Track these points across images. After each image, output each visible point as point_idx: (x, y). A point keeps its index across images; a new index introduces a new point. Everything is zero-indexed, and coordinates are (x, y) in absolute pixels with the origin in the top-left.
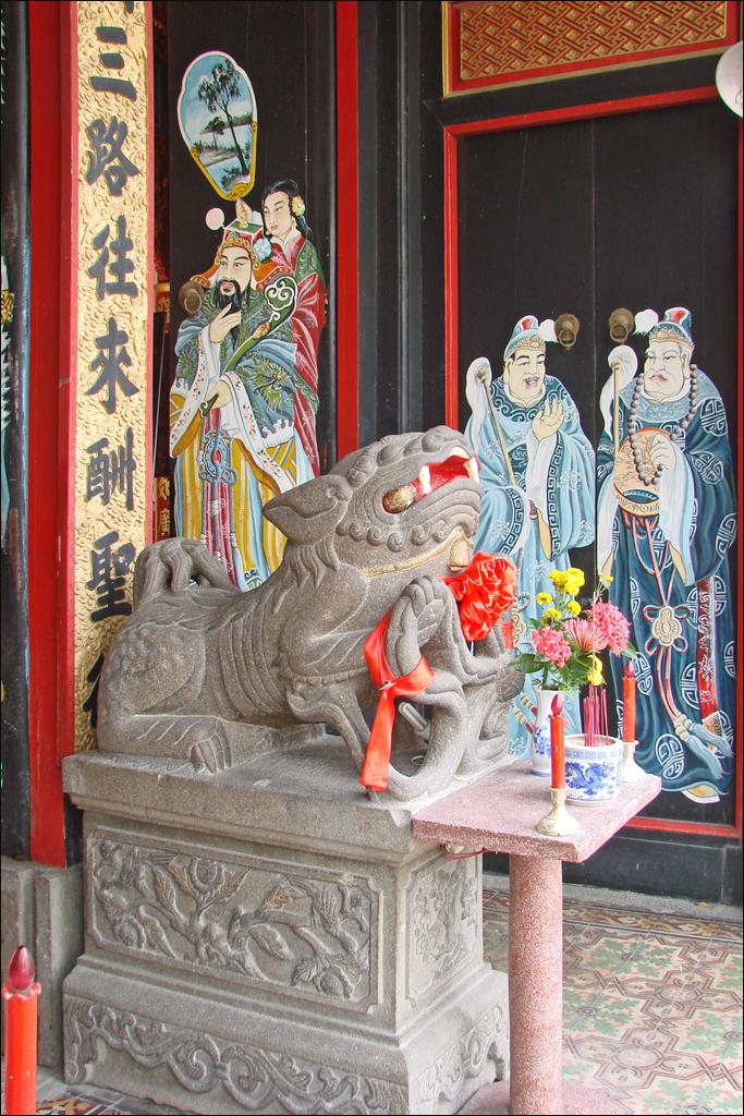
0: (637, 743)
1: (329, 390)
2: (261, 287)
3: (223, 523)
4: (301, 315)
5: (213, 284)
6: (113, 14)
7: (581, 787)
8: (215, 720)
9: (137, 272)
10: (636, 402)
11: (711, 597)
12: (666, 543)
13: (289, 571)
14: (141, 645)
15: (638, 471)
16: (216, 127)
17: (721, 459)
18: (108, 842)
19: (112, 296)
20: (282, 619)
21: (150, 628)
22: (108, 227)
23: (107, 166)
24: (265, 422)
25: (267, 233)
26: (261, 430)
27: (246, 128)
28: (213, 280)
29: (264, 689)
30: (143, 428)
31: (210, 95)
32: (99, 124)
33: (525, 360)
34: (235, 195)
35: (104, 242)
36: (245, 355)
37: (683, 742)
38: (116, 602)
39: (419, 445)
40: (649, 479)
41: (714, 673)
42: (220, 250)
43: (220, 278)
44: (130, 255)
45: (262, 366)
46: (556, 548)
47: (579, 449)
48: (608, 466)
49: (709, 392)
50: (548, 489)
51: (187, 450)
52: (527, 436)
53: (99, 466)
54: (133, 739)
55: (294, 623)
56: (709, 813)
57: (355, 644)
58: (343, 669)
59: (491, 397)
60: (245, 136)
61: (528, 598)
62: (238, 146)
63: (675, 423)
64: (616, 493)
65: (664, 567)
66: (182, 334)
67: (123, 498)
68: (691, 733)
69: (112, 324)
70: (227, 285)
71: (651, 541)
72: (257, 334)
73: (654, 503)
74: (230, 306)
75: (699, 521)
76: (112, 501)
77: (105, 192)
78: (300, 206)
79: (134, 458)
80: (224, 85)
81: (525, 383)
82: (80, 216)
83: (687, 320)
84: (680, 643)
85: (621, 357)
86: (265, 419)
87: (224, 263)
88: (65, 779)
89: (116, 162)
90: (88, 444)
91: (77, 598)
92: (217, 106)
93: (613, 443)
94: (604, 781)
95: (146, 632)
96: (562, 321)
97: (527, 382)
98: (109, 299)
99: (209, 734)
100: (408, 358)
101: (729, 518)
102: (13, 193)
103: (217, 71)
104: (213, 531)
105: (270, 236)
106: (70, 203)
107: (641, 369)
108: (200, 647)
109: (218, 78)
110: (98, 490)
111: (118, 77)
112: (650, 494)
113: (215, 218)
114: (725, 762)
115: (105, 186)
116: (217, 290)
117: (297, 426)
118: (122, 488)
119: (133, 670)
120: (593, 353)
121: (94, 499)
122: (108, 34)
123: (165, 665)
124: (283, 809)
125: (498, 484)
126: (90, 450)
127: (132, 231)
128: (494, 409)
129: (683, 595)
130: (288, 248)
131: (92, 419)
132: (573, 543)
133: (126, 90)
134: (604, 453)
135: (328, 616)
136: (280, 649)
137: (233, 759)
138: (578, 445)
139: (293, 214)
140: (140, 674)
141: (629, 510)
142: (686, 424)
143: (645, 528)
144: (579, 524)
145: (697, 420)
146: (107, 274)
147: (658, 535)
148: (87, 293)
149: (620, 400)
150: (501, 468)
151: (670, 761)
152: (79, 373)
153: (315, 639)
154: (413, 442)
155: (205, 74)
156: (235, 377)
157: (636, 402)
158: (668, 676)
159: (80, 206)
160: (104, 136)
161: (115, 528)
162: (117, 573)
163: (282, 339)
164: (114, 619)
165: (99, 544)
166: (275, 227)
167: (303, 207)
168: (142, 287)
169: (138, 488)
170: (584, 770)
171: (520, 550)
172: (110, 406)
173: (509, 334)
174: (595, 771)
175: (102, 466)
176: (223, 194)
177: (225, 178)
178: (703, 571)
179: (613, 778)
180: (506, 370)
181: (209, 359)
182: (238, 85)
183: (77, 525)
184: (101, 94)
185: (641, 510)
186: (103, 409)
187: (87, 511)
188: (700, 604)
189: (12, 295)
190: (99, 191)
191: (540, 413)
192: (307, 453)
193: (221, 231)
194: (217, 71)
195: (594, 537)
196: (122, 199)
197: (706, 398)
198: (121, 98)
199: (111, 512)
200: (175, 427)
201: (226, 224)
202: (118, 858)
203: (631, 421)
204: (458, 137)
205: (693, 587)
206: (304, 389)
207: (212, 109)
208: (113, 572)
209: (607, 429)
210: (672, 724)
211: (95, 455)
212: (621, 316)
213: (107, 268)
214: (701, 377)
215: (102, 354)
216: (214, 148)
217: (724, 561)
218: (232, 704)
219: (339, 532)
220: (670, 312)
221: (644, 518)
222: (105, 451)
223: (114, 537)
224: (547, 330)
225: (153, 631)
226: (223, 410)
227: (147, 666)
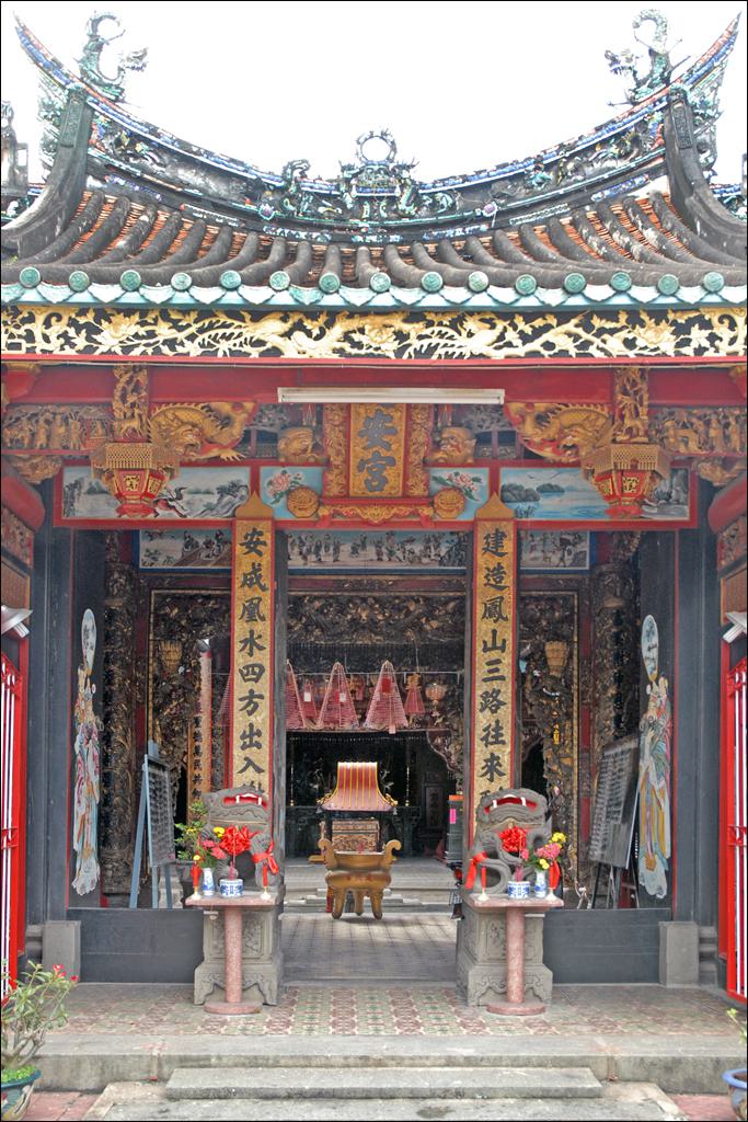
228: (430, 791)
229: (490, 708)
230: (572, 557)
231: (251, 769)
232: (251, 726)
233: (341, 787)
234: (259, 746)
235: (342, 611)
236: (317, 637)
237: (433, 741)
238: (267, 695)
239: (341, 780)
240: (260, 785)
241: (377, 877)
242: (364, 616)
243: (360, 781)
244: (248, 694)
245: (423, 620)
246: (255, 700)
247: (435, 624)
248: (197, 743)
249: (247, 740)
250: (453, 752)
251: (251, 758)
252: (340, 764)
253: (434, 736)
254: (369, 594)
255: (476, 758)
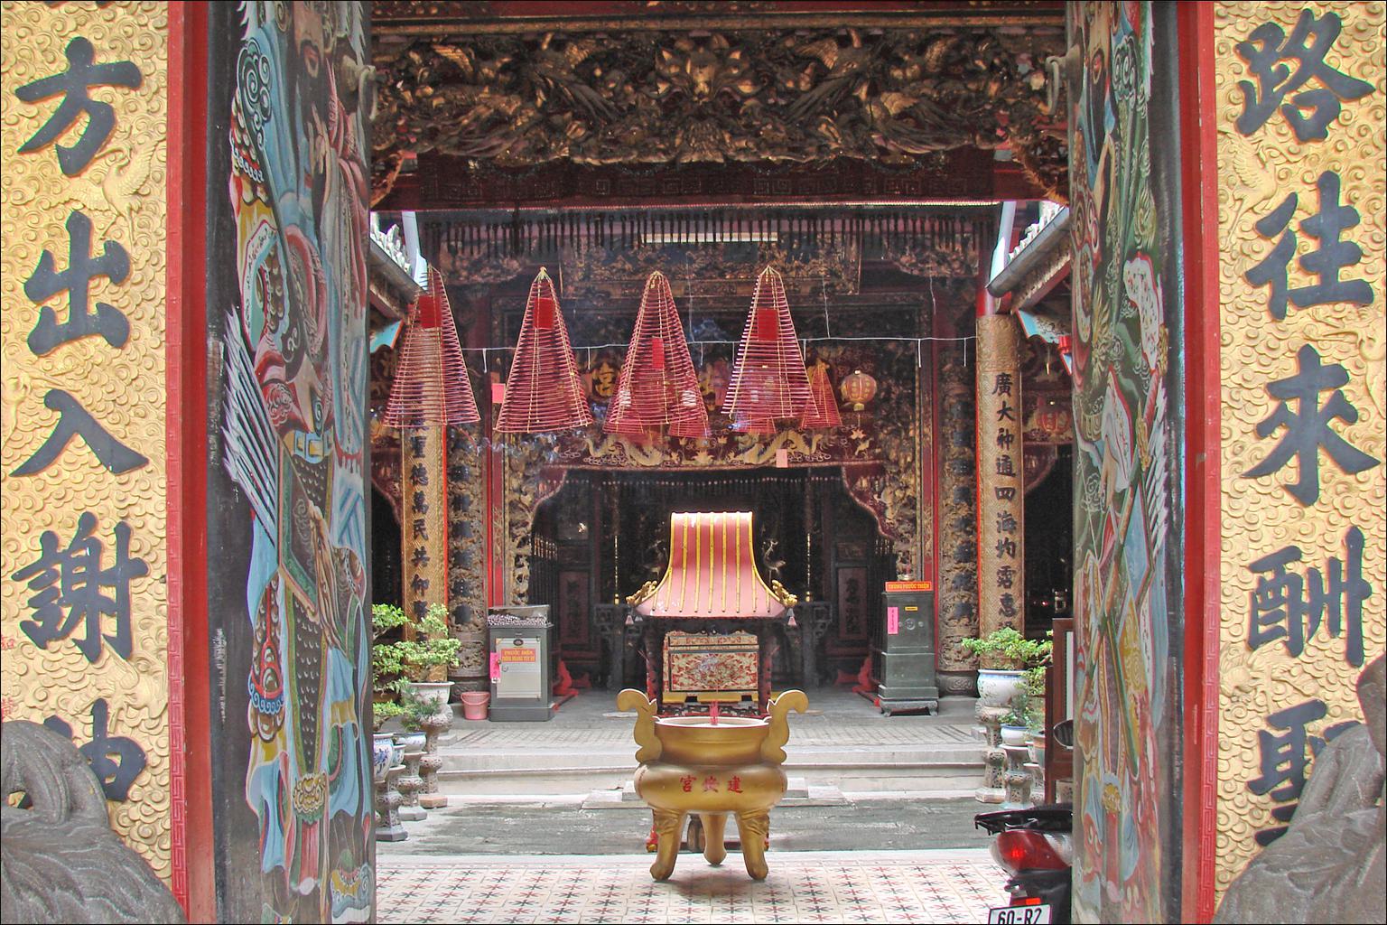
89: (1313, 84)
115: (1285, 129)
118: (1334, 630)
222: (1292, 567)
228: (844, 576)
229: (1291, 116)
231: (79, 450)
232: (79, 226)
233: (678, 565)
234: (116, 329)
235: (643, 76)
236: (576, 146)
237: (853, 481)
238: (156, 66)
239: (679, 550)
240: (123, 532)
241: (756, 783)
242: (702, 80)
243: (718, 552)
244: (61, 65)
245: (862, 93)
246: (98, 94)
247: (893, 103)
248: (418, 489)
249: (60, 304)
250: (888, 502)
251: (85, 394)
252: (678, 519)
253: (855, 474)
254: (715, 24)
255: (1228, 378)
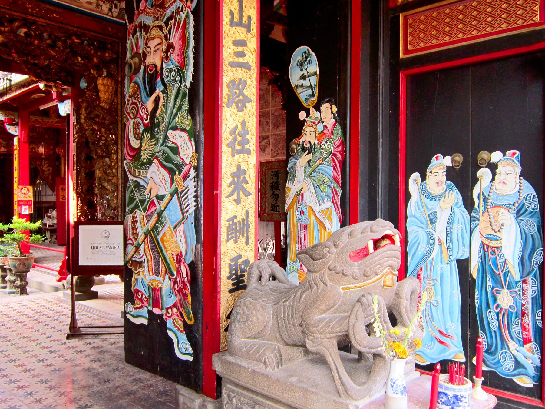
0: (483, 379)
1: (346, 187)
2: (319, 143)
3: (305, 240)
4: (335, 155)
5: (301, 143)
6: (241, 34)
7: (448, 405)
8: (276, 345)
9: (251, 144)
10: (491, 194)
11: (529, 287)
12: (505, 260)
13: (308, 284)
14: (245, 308)
15: (491, 226)
16: (303, 78)
17: (535, 222)
18: (231, 393)
19: (239, 155)
20: (304, 305)
21: (249, 301)
22: (237, 126)
23: (237, 99)
24: (320, 200)
25: (322, 121)
26: (319, 202)
27: (315, 77)
28: (301, 141)
29: (297, 335)
30: (253, 210)
31: (301, 64)
32: (233, 82)
33: (436, 174)
34: (310, 105)
35: (235, 132)
36: (313, 171)
37: (513, 355)
38: (241, 285)
39: (369, 229)
40: (497, 230)
41: (531, 324)
42: (304, 128)
43: (304, 140)
44: (248, 137)
45: (320, 176)
46: (450, 258)
47: (463, 215)
48: (476, 223)
49: (529, 190)
50: (447, 232)
51: (291, 210)
52: (437, 208)
53: (232, 227)
54: (240, 351)
55: (308, 308)
56: (527, 391)
57: (335, 322)
58: (329, 333)
59: (420, 190)
60: (314, 81)
61: (436, 280)
62: (311, 85)
63: (511, 204)
64: (480, 235)
65: (504, 271)
66: (290, 163)
67: (244, 240)
68: (518, 351)
69: (239, 166)
70: (306, 143)
71: (498, 258)
72: (318, 163)
73: (500, 241)
74: (307, 151)
75: (523, 251)
76: (239, 242)
77: (236, 111)
78: (335, 109)
79: (249, 223)
80: (306, 60)
81: (436, 184)
82: (223, 121)
83: (518, 156)
84: (512, 308)
85: (484, 173)
86: (320, 198)
87: (305, 134)
88: (213, 364)
90: (227, 218)
91: (222, 283)
92: (304, 69)
93: (479, 212)
94: (461, 404)
95: (247, 303)
96: (454, 156)
97: (438, 183)
98: (237, 156)
99: (272, 353)
100: (382, 173)
101: (540, 250)
102: (197, 111)
103: (304, 54)
104: (301, 243)
105: (323, 122)
106: (218, 116)
107: (493, 179)
108: (270, 312)
109: (304, 57)
110: (233, 237)
111: (243, 61)
112: (497, 237)
113: (302, 115)
114: (536, 368)
115: (236, 108)
116: (303, 144)
117: (333, 201)
118: (243, 236)
119: (241, 320)
120: (469, 171)
121: (230, 241)
122: (236, 43)
123: (254, 319)
124: (301, 395)
125: (423, 228)
126: (228, 221)
127: (248, 127)
128: (422, 195)
129: (514, 285)
130: (330, 127)
131: (229, 207)
132: (459, 257)
133: (247, 66)
134: (475, 217)
135: (323, 307)
136: (303, 320)
137: (283, 364)
138: (461, 212)
139: (332, 112)
140: (244, 322)
141: (486, 243)
142: (517, 205)
143: (494, 252)
144: (461, 248)
145: (522, 203)
146: (236, 145)
147: (502, 256)
148: (226, 154)
149: (483, 193)
150: (424, 222)
151: (507, 363)
152: (222, 188)
153: (317, 317)
154: (365, 229)
155: (299, 56)
156: (309, 180)
157: (491, 194)
158: (506, 322)
159: (223, 117)
160: (235, 87)
161: (240, 253)
162: (241, 272)
163: (327, 165)
164: (240, 291)
165: (232, 260)
166: (325, 118)
167: (336, 109)
168: (253, 150)
169: (251, 236)
170: (450, 397)
171: (433, 258)
172: (238, 201)
173: (429, 162)
174: (456, 398)
175: (234, 227)
176: (305, 105)
177: (306, 98)
178: (525, 274)
179: (466, 403)
180: (427, 178)
181: (300, 172)
182: (312, 59)
183: (222, 252)
184: (234, 69)
185: (492, 244)
186: (234, 203)
187: (227, 247)
188: (523, 290)
189: (197, 154)
190: (233, 110)
191: (443, 198)
192: (337, 213)
193: (304, 120)
194: (304, 54)
195: (469, 255)
196: (244, 113)
197: (527, 193)
198: (244, 70)
199: (238, 246)
200: (287, 200)
201: (306, 117)
202: (235, 401)
203: (488, 203)
204: (407, 76)
205: (520, 281)
206: (335, 185)
207: (301, 70)
208: (239, 272)
209: (476, 206)
210: (508, 346)
211: (231, 223)
212: (484, 155)
213: (236, 143)
214: (525, 183)
215: (234, 179)
216: (302, 86)
217: (536, 271)
218: (283, 339)
219: (329, 269)
220: (509, 153)
221: (494, 247)
222: (236, 221)
223: (240, 257)
224: (447, 161)
225: (251, 303)
226: (305, 194)
227: (247, 319)
230: (117, 10)
